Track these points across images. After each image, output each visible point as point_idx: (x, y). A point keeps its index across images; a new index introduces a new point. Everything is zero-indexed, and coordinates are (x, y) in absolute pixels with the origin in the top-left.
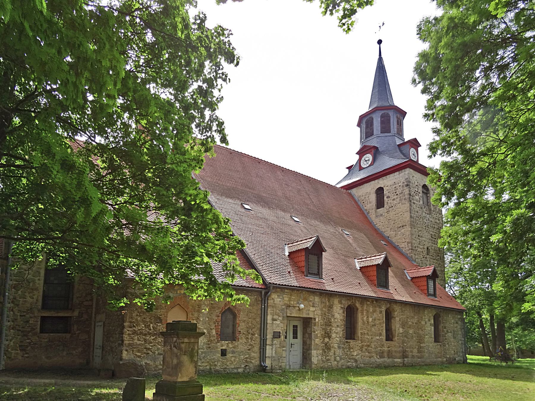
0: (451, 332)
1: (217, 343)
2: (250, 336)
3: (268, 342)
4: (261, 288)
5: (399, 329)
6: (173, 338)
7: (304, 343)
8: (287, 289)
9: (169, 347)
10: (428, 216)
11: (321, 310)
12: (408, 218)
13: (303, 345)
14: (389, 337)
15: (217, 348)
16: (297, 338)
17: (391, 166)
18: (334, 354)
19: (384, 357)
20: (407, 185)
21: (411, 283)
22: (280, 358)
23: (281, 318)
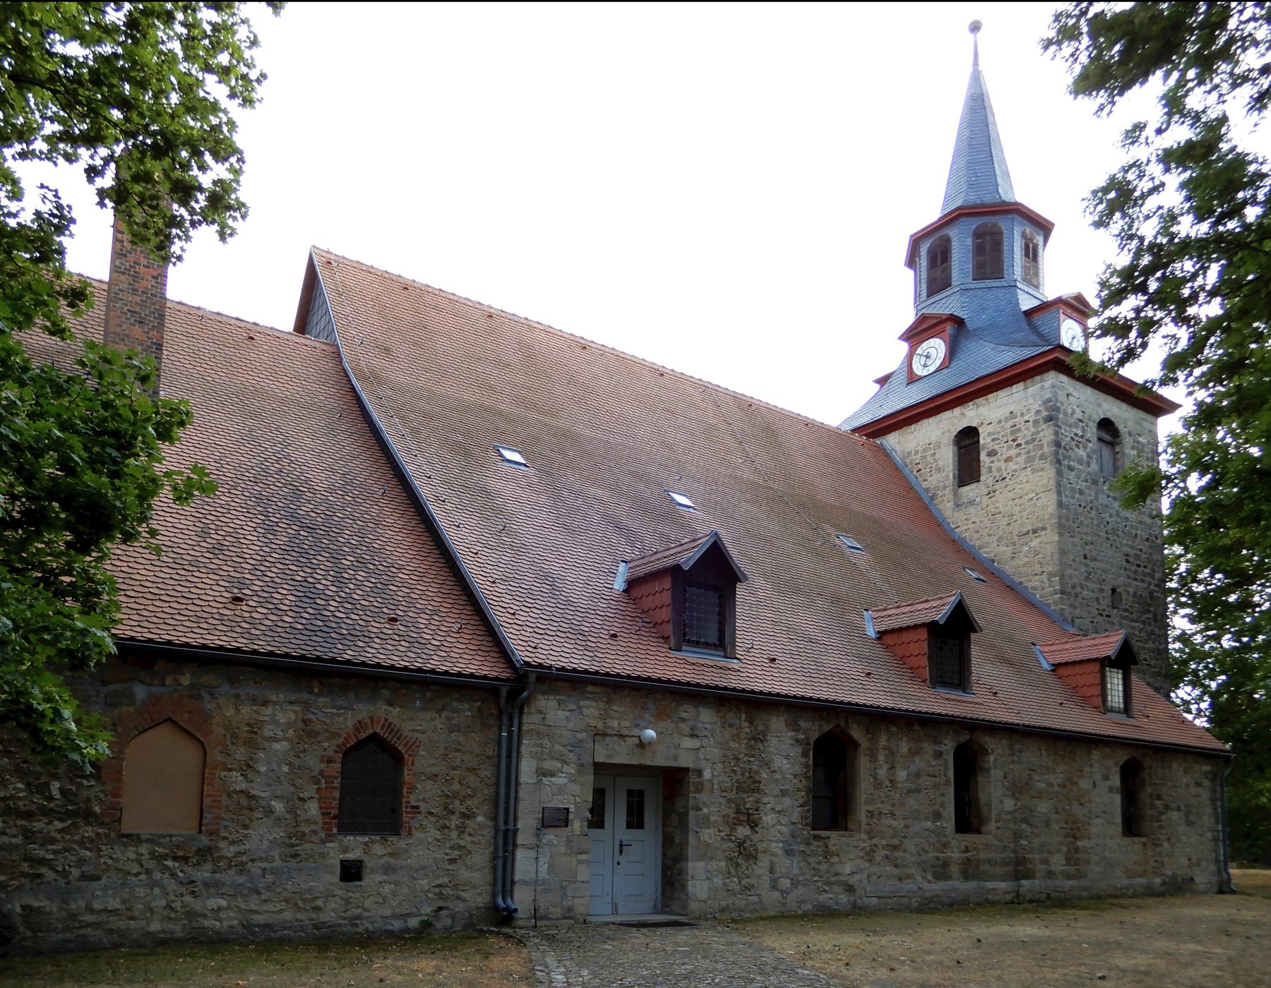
0: (1179, 809)
1: (323, 842)
2: (454, 821)
4: (497, 679)
5: (1001, 802)
7: (668, 841)
12: (1052, 508)
13: (664, 846)
14: (968, 818)
16: (640, 826)
17: (1001, 366)
18: (772, 871)
20: (1049, 419)
21: (1050, 679)
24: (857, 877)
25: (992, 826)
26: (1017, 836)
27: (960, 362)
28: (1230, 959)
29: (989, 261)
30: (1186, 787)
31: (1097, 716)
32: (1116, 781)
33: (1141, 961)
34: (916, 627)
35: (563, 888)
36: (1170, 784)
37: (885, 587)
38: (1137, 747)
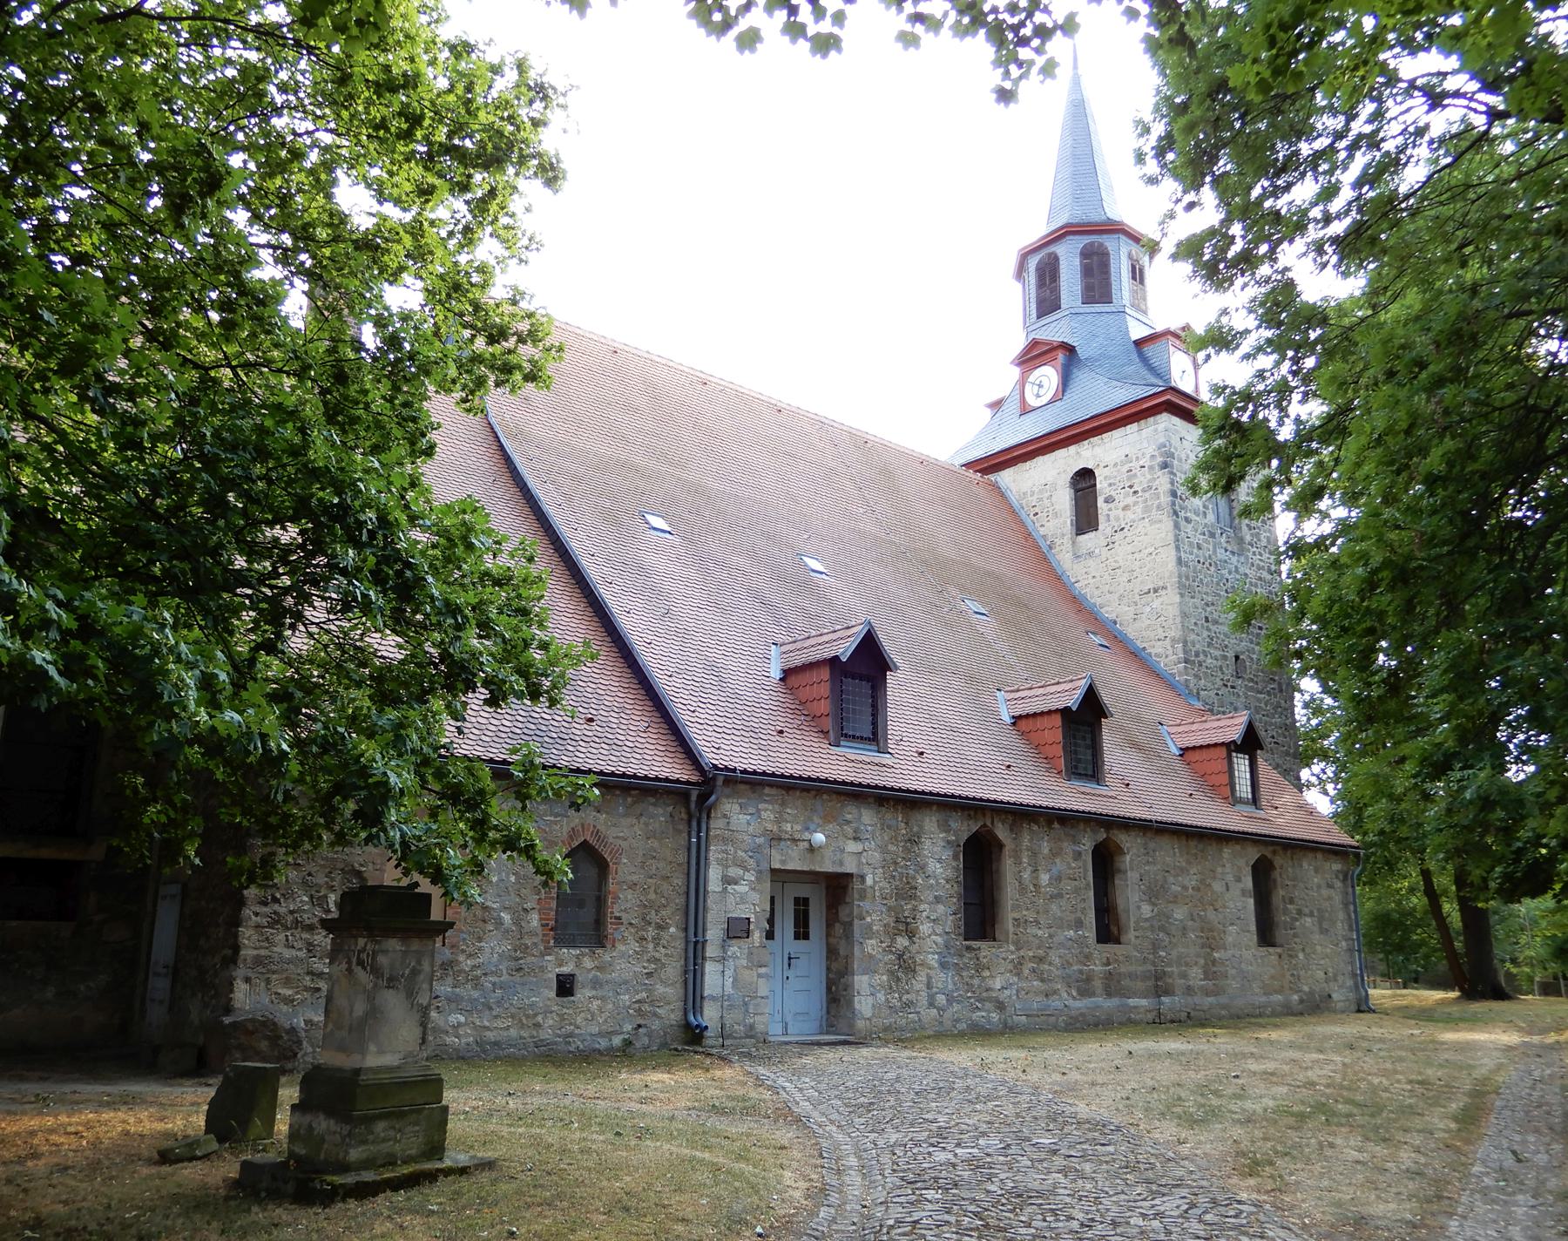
0: (1311, 915)
1: (543, 955)
2: (651, 932)
3: (711, 951)
4: (688, 783)
5: (1139, 908)
6: (356, 937)
7: (832, 953)
8: (771, 785)
9: (344, 966)
10: (1234, 559)
11: (883, 850)
12: (1172, 565)
14: (1108, 928)
15: (542, 969)
16: (806, 937)
19: (1093, 994)
20: (1165, 466)
21: (1179, 765)
22: (748, 999)
23: (751, 876)
24: (1007, 992)
25: (1130, 935)
26: (1156, 946)
27: (1074, 393)
28: (1344, 1064)
29: (1097, 286)
30: (1312, 888)
31: (1226, 807)
32: (1248, 882)
33: (1270, 1066)
34: (1050, 712)
35: (746, 1004)
36: (1301, 885)
37: (1013, 660)
38: (1266, 843)
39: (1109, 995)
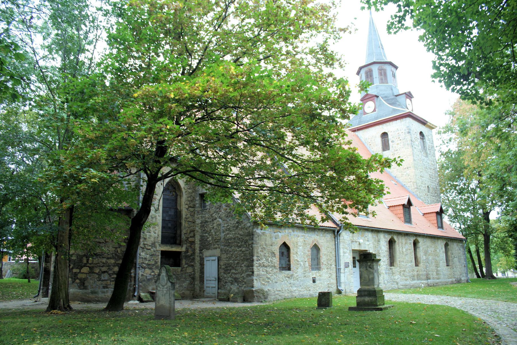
3: (342, 271)
14: (417, 265)
19: (415, 280)
20: (409, 133)
39: (418, 280)
